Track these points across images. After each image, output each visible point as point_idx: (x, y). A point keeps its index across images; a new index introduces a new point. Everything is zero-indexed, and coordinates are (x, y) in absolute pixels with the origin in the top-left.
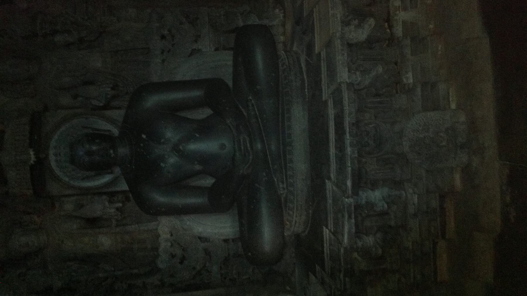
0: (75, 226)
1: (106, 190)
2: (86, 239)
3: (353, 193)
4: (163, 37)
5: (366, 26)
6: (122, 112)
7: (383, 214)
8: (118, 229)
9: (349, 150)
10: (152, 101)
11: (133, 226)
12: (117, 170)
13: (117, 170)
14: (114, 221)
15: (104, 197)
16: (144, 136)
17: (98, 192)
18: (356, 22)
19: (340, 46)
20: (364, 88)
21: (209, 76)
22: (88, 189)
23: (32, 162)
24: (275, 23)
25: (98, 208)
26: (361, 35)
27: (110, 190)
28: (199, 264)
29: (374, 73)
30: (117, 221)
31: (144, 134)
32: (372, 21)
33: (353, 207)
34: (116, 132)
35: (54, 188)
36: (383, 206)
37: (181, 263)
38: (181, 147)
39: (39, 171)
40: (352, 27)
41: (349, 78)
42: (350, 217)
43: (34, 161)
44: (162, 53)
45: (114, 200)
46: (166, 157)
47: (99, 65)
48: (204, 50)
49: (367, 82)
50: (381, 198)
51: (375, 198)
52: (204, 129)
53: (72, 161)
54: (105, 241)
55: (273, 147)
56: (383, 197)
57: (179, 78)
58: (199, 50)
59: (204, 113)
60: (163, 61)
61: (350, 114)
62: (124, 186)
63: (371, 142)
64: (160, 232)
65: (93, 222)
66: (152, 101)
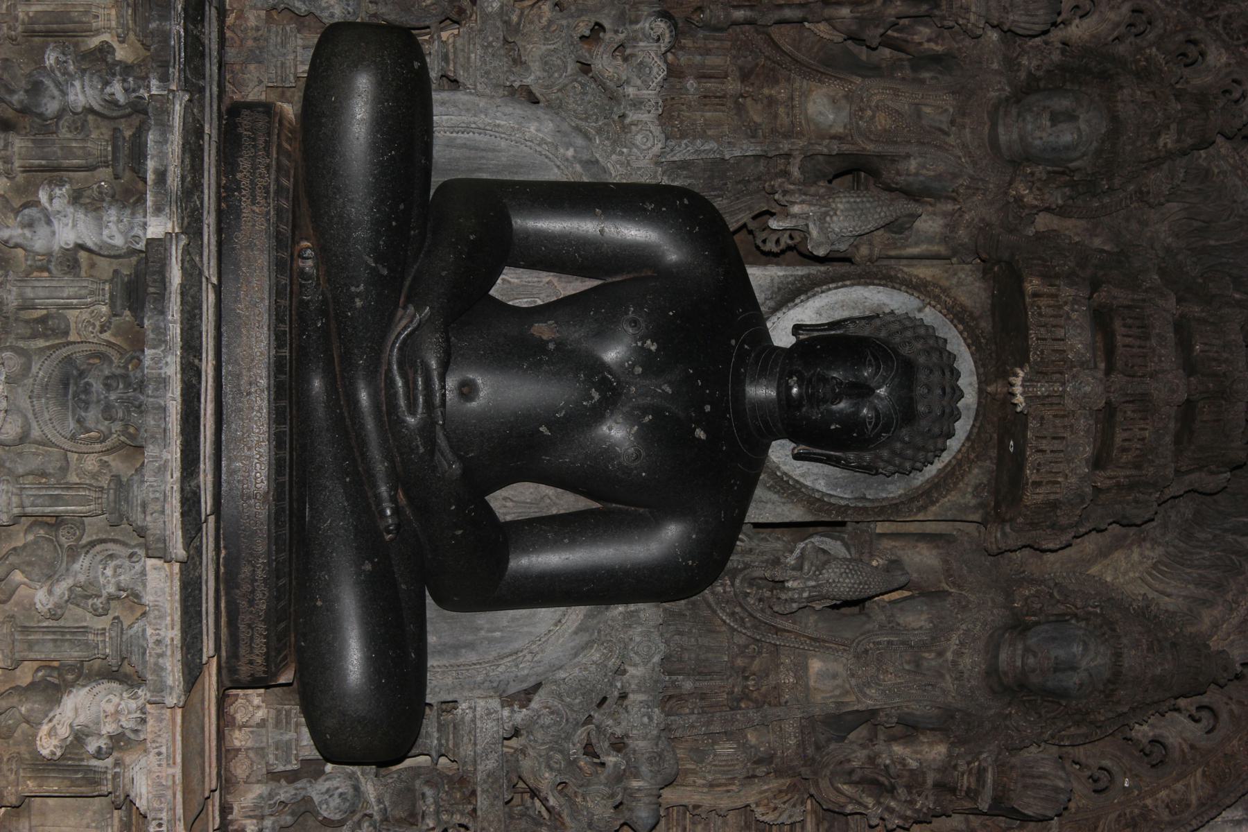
0: (913, 165)
1: (815, 270)
2: (883, 121)
3: (167, 250)
4: (619, 745)
5: (64, 732)
6: (755, 514)
7: (52, 172)
8: (785, 146)
9: (172, 368)
10: (666, 539)
11: (737, 153)
12: (781, 334)
13: (781, 334)
14: (795, 172)
15: (821, 252)
16: (700, 434)
17: (841, 266)
18: (92, 746)
19: (168, 666)
20: (92, 544)
21: (483, 619)
22: (867, 277)
23: (1021, 374)
24: (258, 790)
25: (837, 220)
26: (83, 706)
27: (801, 271)
28: (544, 21)
29: (62, 588)
30: (785, 174)
31: (700, 439)
32: (47, 746)
33: (149, 203)
34: (780, 453)
35: (970, 288)
36: (51, 199)
37: (599, 27)
38: (596, 396)
39: (1004, 339)
40: (109, 728)
41: (143, 573)
42: (161, 176)
43: (1016, 375)
44: (623, 696)
45: (791, 237)
46: (639, 370)
47: (816, 665)
48: (495, 703)
49: (83, 563)
50: (55, 222)
51: (74, 226)
52: (518, 449)
53: (908, 369)
54: (822, 107)
55: (317, 383)
56: (49, 222)
57: (576, 614)
58: (508, 701)
59: (514, 501)
60: (620, 672)
61: (162, 469)
62: (761, 277)
63: (97, 386)
64: (657, 130)
65: (852, 169)
66: (666, 539)
